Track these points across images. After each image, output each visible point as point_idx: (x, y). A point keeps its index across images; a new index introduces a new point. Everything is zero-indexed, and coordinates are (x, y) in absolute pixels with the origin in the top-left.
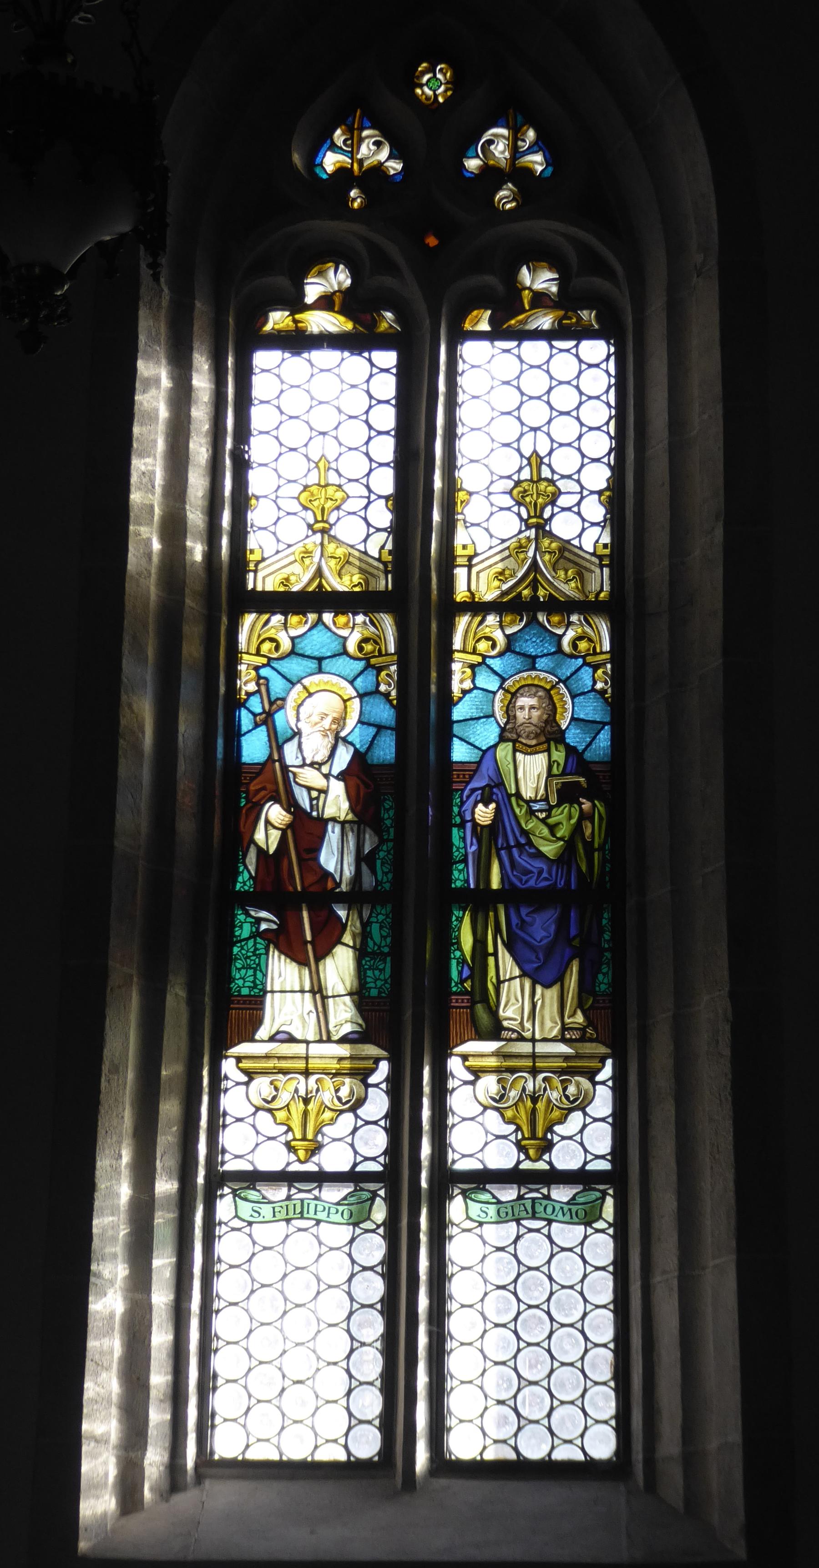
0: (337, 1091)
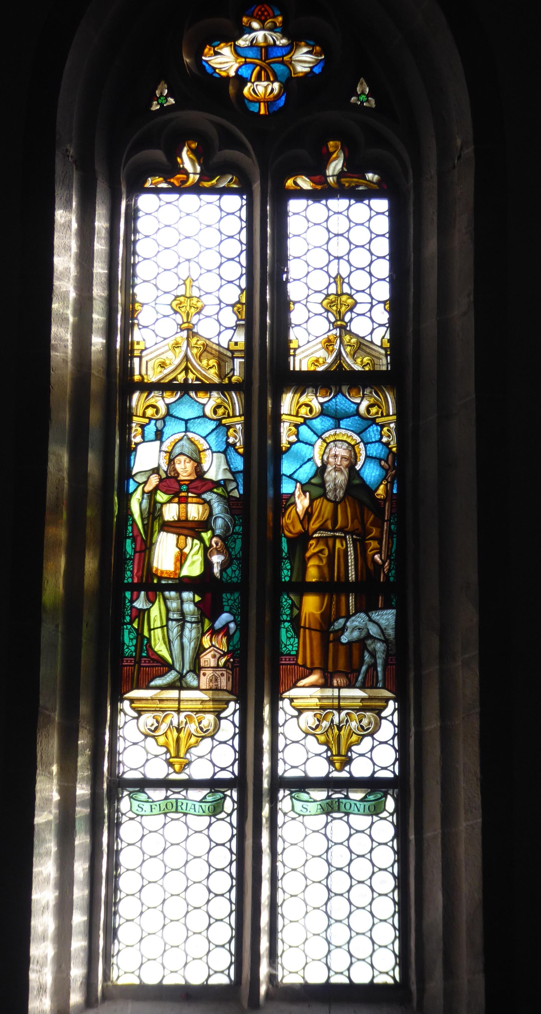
0: (200, 723)
